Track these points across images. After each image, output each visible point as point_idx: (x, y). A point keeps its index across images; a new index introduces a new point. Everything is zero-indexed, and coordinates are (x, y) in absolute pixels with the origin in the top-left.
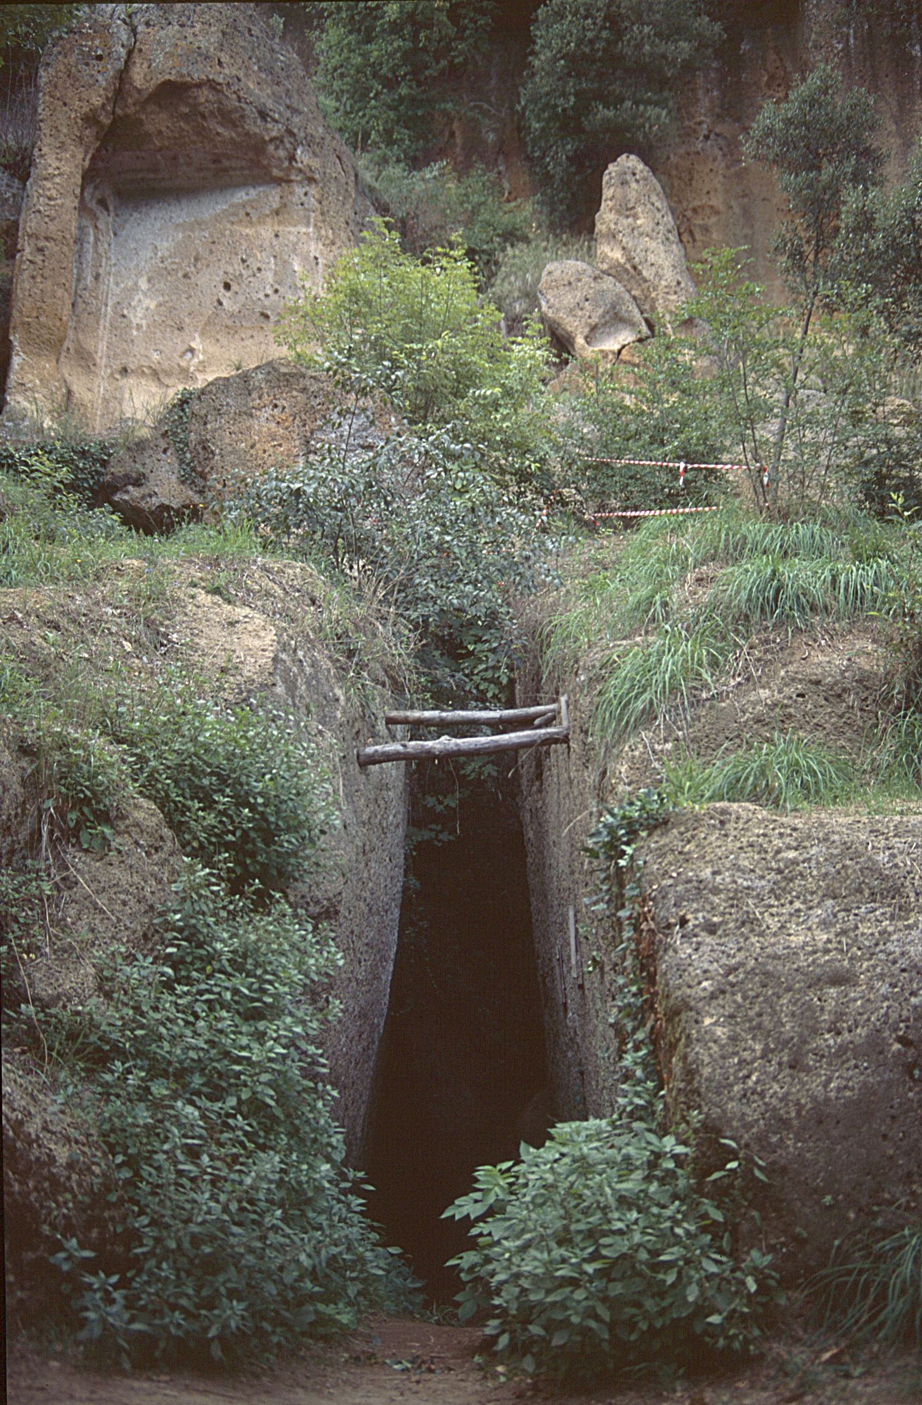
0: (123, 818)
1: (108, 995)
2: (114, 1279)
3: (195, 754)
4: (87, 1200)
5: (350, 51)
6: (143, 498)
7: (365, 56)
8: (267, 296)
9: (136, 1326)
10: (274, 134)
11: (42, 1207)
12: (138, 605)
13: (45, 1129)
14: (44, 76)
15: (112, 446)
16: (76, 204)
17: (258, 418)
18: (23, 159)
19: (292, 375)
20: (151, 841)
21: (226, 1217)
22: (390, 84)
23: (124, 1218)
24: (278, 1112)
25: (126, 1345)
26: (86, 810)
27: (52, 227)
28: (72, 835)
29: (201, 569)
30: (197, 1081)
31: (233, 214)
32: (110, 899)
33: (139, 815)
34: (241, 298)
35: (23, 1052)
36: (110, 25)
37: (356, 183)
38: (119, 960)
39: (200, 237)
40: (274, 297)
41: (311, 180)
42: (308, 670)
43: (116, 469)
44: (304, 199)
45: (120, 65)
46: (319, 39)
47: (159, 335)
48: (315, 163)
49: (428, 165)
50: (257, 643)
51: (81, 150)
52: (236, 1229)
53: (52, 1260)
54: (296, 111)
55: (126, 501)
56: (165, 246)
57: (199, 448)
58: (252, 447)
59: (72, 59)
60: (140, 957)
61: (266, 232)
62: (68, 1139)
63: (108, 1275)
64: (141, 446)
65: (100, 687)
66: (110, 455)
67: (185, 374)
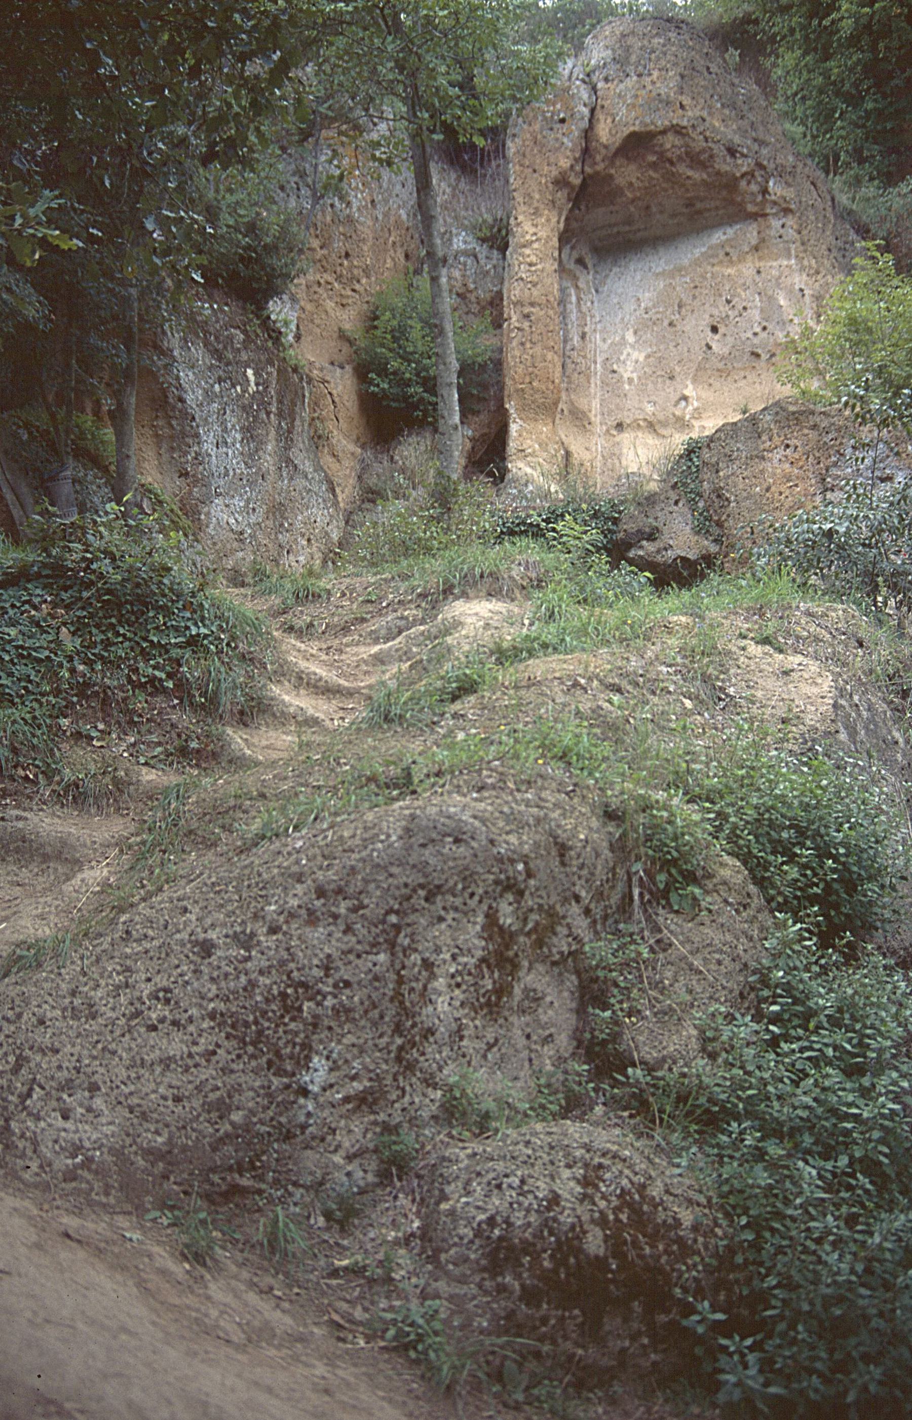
0: (710, 876)
1: (713, 1056)
2: (749, 1342)
3: (772, 807)
4: (714, 1262)
5: (809, 72)
6: (658, 552)
7: (826, 74)
8: (755, 334)
9: (773, 1390)
10: (744, 169)
11: (673, 1270)
12: (692, 662)
13: (667, 1192)
14: (512, 147)
15: (621, 503)
16: (556, 266)
17: (771, 460)
18: (499, 230)
19: (801, 413)
20: (739, 898)
21: (854, 1278)
22: (855, 100)
23: (749, 1281)
24: (889, 1171)
25: (766, 1410)
26: (673, 871)
27: (535, 292)
28: (662, 896)
29: (746, 619)
30: (807, 1140)
31: (712, 256)
32: (705, 959)
33: (726, 873)
34: (730, 340)
35: (631, 1116)
36: (569, 88)
37: (834, 207)
38: (720, 1020)
39: (682, 285)
40: (764, 335)
41: (787, 211)
42: (865, 714)
43: (628, 526)
44: (782, 231)
45: (585, 124)
46: (775, 65)
47: (650, 386)
48: (790, 193)
49: (903, 179)
50: (815, 690)
51: (555, 213)
52: (863, 1291)
53: (685, 1323)
54: (762, 143)
55: (641, 557)
56: (647, 297)
57: (713, 496)
58: (768, 490)
59: (537, 127)
60: (738, 1016)
61: (747, 269)
62: (690, 1202)
63: (743, 1338)
64: (651, 500)
65: (670, 746)
66: (620, 512)
67: (682, 424)
